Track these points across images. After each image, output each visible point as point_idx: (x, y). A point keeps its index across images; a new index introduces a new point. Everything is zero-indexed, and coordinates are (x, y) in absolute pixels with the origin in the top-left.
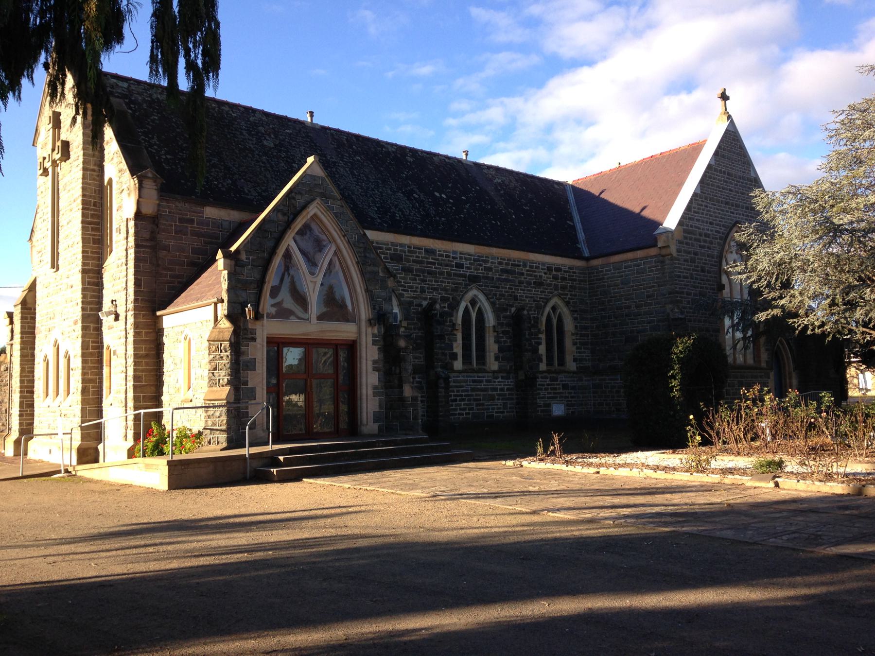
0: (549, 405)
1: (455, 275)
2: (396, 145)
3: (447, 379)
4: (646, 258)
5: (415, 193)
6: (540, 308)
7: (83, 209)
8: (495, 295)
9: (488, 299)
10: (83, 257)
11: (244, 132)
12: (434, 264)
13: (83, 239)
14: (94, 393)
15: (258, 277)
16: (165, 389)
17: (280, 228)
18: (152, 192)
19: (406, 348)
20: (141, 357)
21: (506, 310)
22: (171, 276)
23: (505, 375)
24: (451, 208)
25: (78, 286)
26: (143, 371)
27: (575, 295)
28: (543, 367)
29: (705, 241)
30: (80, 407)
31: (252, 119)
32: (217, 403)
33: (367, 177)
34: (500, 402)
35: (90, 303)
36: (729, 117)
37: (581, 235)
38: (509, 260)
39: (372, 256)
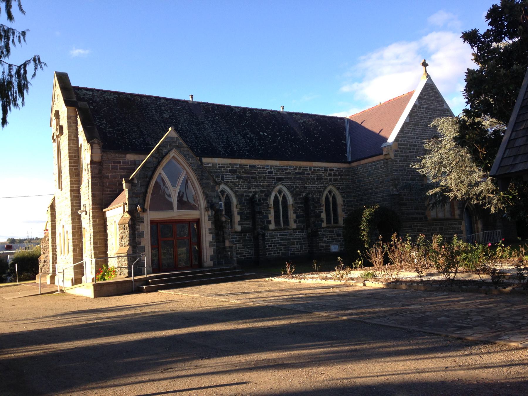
0: (329, 246)
1: (268, 178)
2: (241, 108)
3: (263, 235)
4: (379, 161)
5: (248, 134)
6: (321, 192)
7: (69, 159)
8: (293, 187)
9: (288, 189)
10: (71, 183)
11: (153, 111)
12: (255, 173)
13: (70, 174)
14: (79, 251)
15: (144, 190)
16: (108, 248)
17: (155, 165)
18: (97, 148)
19: (226, 221)
20: (97, 232)
21: (299, 195)
22: (110, 191)
23: (300, 230)
24: (269, 141)
25: (69, 198)
26: (98, 239)
27: (343, 184)
28: (324, 225)
29: (414, 149)
30: (72, 258)
31: (158, 103)
32: (123, 255)
33: (221, 128)
34: (299, 246)
35: (75, 206)
36: (428, 76)
37: (349, 149)
38: (300, 167)
39: (206, 175)
